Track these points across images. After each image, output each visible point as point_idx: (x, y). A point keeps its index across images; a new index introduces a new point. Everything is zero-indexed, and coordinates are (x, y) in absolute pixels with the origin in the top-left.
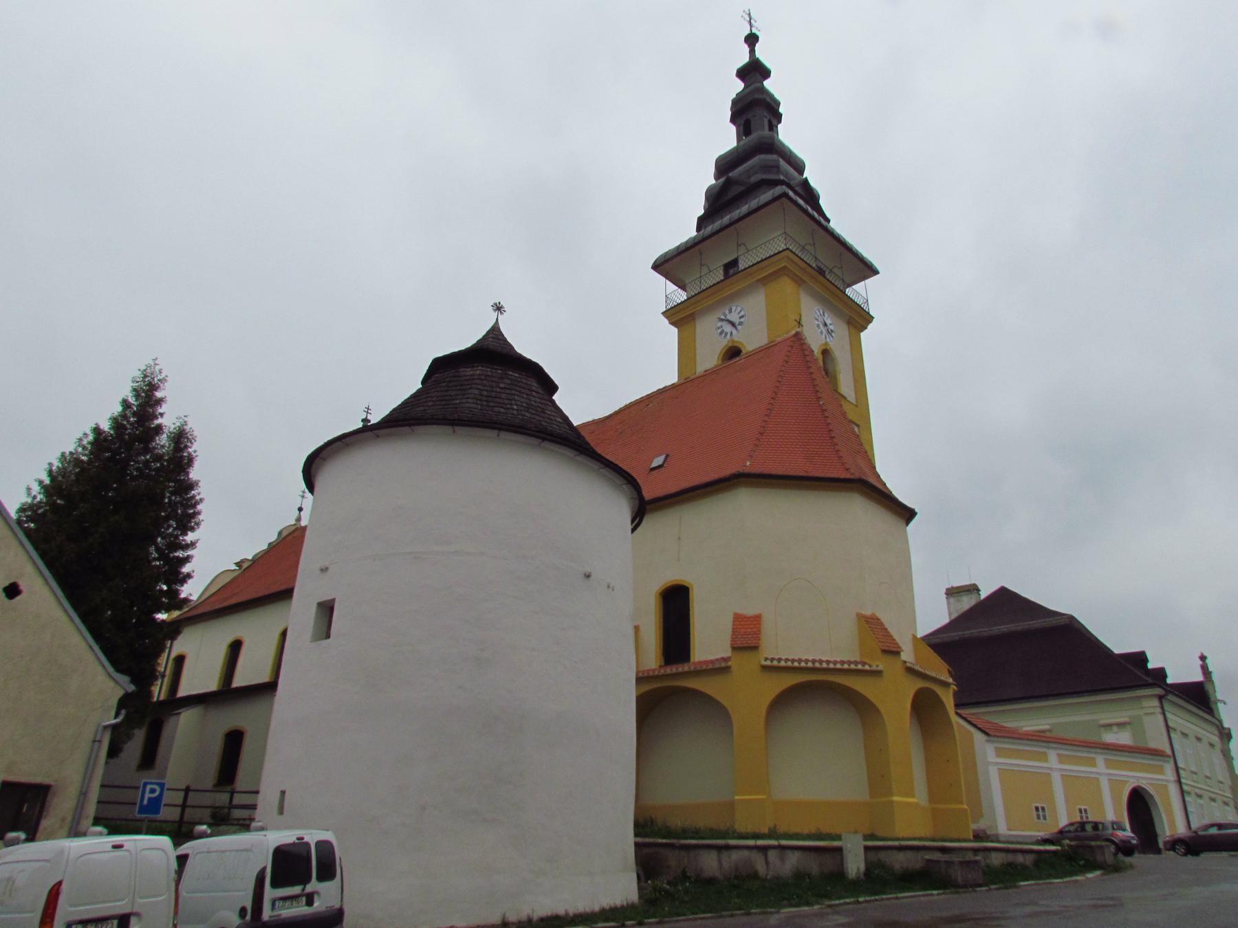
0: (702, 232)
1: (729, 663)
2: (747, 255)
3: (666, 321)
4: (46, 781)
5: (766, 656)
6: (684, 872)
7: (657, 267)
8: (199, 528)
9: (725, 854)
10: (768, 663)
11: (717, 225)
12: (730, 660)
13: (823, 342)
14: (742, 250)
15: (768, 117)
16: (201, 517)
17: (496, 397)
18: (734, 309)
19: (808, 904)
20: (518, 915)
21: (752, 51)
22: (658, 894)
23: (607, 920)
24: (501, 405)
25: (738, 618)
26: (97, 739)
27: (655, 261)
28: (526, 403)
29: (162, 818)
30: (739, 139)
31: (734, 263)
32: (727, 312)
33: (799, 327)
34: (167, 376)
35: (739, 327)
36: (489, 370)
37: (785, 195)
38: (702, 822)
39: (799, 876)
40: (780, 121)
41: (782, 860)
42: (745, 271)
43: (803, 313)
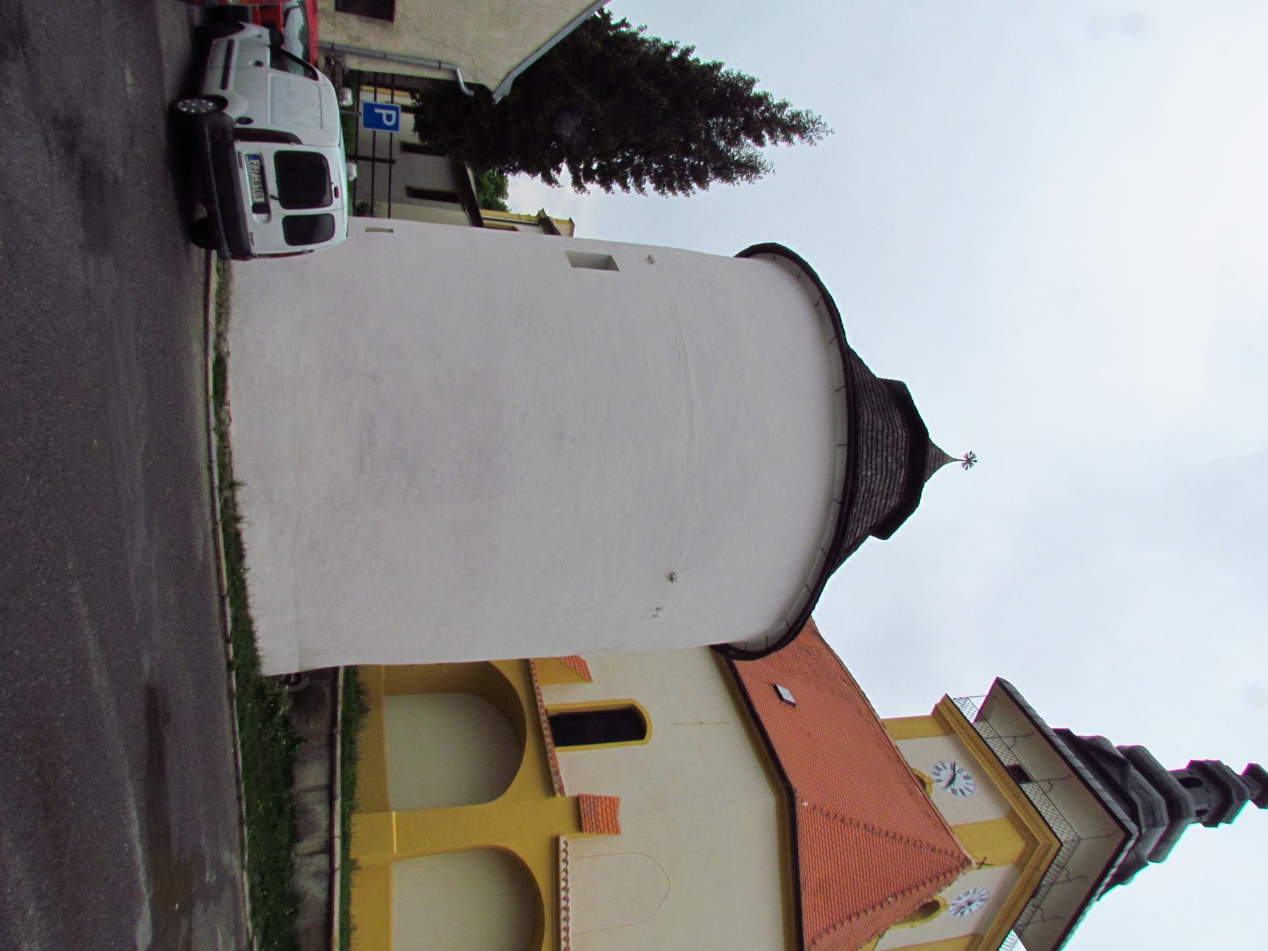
0: (1054, 734)
1: (558, 795)
2: (1041, 792)
3: (938, 700)
4: (398, 15)
5: (569, 843)
6: (300, 740)
7: (1000, 684)
8: (660, 194)
9: (322, 795)
10: (562, 846)
11: (1068, 752)
12: (561, 795)
13: (948, 902)
14: (1046, 787)
15: (1209, 809)
16: (670, 194)
17: (877, 450)
18: (970, 781)
19: (254, 912)
22: (270, 699)
23: (235, 620)
24: (870, 455)
25: (613, 803)
26: (442, 65)
27: (1006, 682)
28: (873, 490)
29: (360, 130)
30: (1174, 773)
31: (1027, 779)
32: (965, 774)
33: (977, 864)
34: (815, 144)
35: (949, 790)
36: (904, 444)
37: (1128, 835)
38: (363, 770)
39: (294, 900)
40: (1206, 824)
41: (316, 875)
42: (1020, 791)
43: (996, 868)
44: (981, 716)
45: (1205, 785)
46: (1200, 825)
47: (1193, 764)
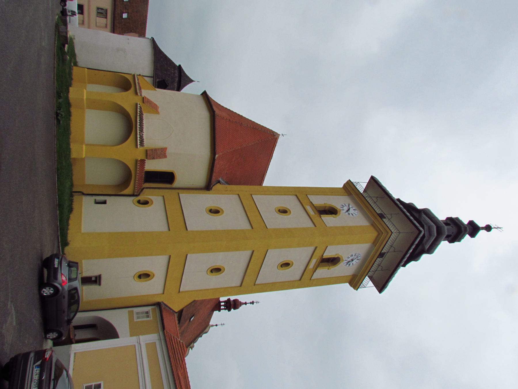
7: (373, 178)
13: (343, 259)
18: (356, 211)
20: (70, 241)
21: (483, 228)
27: (374, 177)
30: (442, 220)
35: (347, 213)
37: (420, 232)
44: (365, 191)
45: (452, 225)
46: (446, 242)
47: (448, 219)
